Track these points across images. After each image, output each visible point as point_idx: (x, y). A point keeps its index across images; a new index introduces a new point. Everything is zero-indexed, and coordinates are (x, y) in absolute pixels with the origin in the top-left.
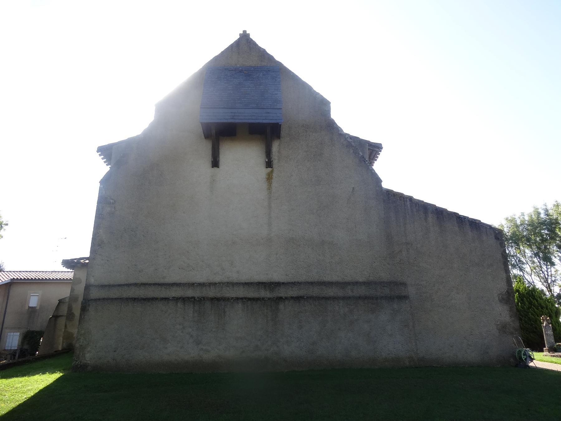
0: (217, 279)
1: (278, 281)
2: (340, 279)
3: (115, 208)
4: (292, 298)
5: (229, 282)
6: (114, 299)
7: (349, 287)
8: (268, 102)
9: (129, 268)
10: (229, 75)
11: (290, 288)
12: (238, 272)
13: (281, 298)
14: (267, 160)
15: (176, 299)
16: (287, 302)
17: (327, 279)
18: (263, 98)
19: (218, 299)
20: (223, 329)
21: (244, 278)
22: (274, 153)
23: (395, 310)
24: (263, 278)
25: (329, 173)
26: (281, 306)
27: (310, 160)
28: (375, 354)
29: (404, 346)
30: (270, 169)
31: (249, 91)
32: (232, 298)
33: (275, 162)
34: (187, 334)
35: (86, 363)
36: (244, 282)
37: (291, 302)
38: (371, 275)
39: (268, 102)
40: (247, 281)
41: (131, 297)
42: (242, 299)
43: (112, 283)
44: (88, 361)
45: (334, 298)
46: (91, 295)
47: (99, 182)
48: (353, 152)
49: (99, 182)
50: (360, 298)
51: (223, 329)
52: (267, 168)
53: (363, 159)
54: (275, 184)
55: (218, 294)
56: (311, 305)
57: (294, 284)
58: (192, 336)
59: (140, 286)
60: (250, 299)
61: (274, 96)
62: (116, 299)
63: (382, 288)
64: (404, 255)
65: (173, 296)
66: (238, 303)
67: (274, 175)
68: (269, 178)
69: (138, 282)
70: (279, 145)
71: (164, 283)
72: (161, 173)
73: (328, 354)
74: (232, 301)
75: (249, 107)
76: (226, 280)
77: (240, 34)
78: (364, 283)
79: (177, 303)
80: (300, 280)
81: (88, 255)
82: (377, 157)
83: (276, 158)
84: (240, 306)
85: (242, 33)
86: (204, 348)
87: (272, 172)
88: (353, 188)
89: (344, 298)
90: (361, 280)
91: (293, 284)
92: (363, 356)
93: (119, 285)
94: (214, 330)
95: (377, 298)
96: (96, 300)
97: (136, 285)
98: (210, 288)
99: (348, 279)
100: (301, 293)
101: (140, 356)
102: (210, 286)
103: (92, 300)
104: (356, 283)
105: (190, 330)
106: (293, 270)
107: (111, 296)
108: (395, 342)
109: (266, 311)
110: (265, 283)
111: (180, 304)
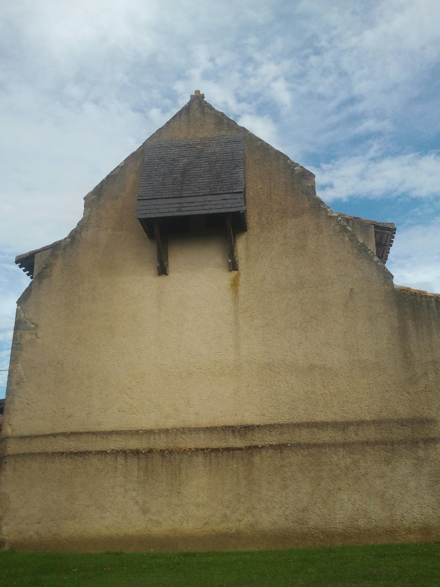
0: (170, 424)
1: (251, 423)
2: (338, 419)
3: (36, 334)
4: (271, 446)
5: (185, 427)
6: (37, 453)
7: (351, 428)
8: (225, 185)
9: (55, 412)
10: (176, 153)
11: (268, 433)
12: (197, 414)
13: (256, 447)
14: (230, 261)
15: (116, 453)
16: (264, 453)
17: (320, 417)
18: (219, 179)
19: (171, 452)
20: (179, 493)
21: (205, 422)
22: (239, 251)
23: (421, 458)
24: (230, 421)
25: (315, 272)
26: (257, 459)
27: (289, 255)
28: (392, 523)
29: (436, 511)
30: (234, 273)
31: (202, 172)
32: (190, 449)
33: (242, 263)
34: (130, 498)
35: (3, 539)
36: (205, 426)
37: (269, 452)
38: (383, 410)
39: (225, 185)
40: (209, 426)
41: (58, 451)
42: (203, 450)
43: (34, 433)
44: (6, 535)
45: (334, 445)
46: (9, 449)
47: (16, 303)
48: (350, 239)
49: (16, 303)
50: (367, 443)
51: (179, 493)
52: (231, 271)
53: (364, 248)
54: (242, 291)
55: (170, 444)
56: (298, 455)
57: (274, 427)
58: (137, 503)
59: (69, 435)
60: (217, 450)
61: (233, 175)
62: (39, 454)
63: (400, 427)
64: (431, 379)
65: (113, 447)
66: (197, 456)
67: (242, 279)
68: (235, 284)
69: (67, 431)
70: (247, 239)
71: (100, 431)
72: (94, 286)
73: (325, 525)
74: (189, 453)
75: (201, 194)
76: (180, 425)
77: (192, 96)
78: (374, 422)
79: (117, 457)
80: (281, 422)
81: (201, 93)
82: (392, 242)
83: (243, 256)
84: (199, 459)
85: (194, 94)
86: (154, 518)
87: (238, 276)
88: (351, 289)
89: (344, 445)
90: (368, 418)
91: (271, 427)
92: (21, 321)
93: (44, 436)
94: (166, 494)
95: (392, 443)
96: (14, 456)
97: (64, 434)
98: (160, 436)
99: (350, 417)
100: (286, 438)
101: (71, 528)
102: (159, 434)
103: (9, 455)
104: (360, 423)
105: (134, 494)
106: (271, 407)
107: (33, 450)
108: (423, 505)
109: (236, 466)
110: (233, 427)
111: (121, 460)
